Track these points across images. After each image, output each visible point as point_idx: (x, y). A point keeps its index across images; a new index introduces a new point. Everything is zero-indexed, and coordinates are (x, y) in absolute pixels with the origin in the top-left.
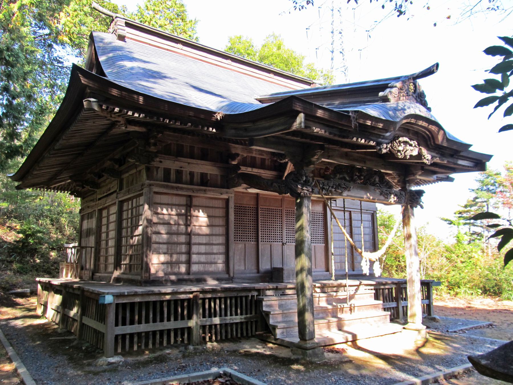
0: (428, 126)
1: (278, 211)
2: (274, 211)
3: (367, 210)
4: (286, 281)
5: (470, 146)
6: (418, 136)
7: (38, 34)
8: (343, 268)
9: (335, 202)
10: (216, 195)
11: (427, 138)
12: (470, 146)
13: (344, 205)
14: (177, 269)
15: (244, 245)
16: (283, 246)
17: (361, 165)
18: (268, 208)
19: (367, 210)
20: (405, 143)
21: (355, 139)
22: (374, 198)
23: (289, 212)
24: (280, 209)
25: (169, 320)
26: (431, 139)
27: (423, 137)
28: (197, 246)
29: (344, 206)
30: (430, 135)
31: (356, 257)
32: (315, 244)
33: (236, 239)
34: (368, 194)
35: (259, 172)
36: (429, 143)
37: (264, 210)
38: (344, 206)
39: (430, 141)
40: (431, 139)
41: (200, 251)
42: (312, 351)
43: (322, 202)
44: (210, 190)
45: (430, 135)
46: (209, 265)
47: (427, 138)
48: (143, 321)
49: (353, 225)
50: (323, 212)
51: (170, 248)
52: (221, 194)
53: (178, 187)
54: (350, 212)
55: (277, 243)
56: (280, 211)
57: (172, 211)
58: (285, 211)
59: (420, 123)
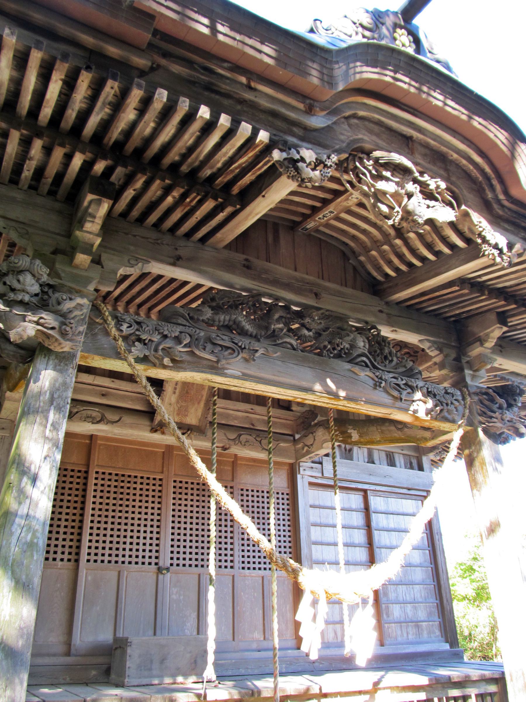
1: (152, 482)
2: (139, 480)
3: (409, 489)
4: (135, 682)
6: (446, 170)
7: (77, 313)
8: (339, 640)
9: (319, 466)
11: (481, 179)
13: (335, 471)
15: (116, 574)
16: (161, 577)
18: (121, 473)
19: (409, 489)
22: (353, 394)
23: (184, 485)
24: (158, 477)
26: (495, 182)
27: (468, 175)
29: (335, 475)
30: (488, 169)
31: (387, 608)
32: (262, 572)
33: (223, 564)
35: (96, 382)
36: (490, 195)
37: (107, 477)
38: (335, 475)
39: (492, 187)
40: (495, 182)
43: (286, 468)
45: (488, 169)
47: (481, 179)
49: (374, 524)
50: (288, 491)
54: (365, 491)
55: (251, 571)
56: (158, 483)
58: (173, 484)
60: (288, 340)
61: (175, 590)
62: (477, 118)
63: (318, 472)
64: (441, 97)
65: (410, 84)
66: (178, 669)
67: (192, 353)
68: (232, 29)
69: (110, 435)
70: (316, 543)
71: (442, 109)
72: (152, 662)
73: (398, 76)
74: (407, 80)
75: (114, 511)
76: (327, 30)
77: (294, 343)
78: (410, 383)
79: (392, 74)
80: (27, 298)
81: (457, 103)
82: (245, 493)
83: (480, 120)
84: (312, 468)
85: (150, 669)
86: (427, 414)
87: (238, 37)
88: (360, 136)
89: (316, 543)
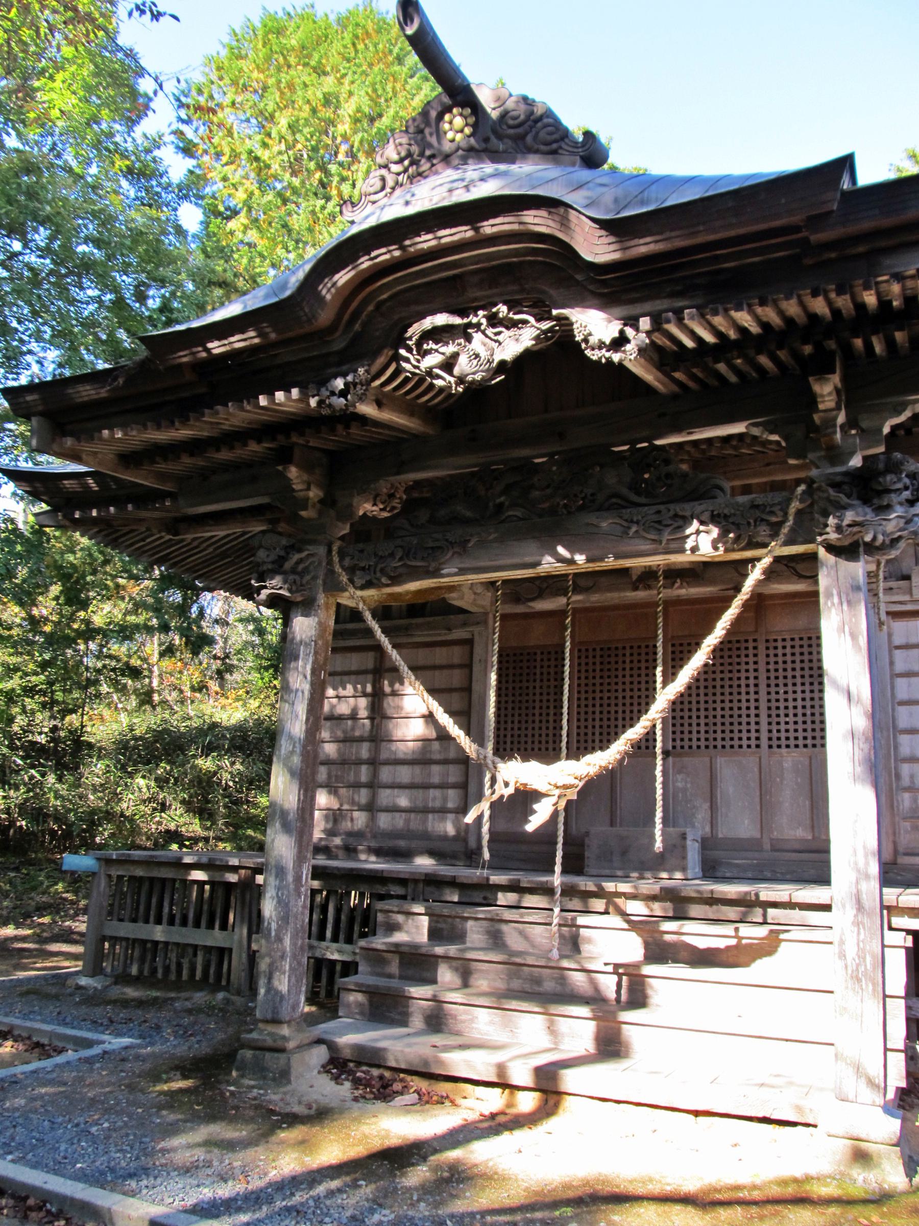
0: (477, 230)
4: (594, 872)
5: (846, 163)
10: (440, 635)
12: (846, 163)
14: (349, 824)
17: (544, 451)
20: (438, 334)
21: (263, 401)
22: (597, 553)
25: (210, 926)
28: (391, 768)
34: (561, 550)
41: (398, 780)
42: (254, 1056)
44: (418, 626)
46: (436, 815)
48: (203, 923)
51: (334, 773)
52: (449, 629)
53: (346, 630)
55: (792, 749)
57: (344, 688)
59: (425, 241)
60: (511, 513)
61: (679, 777)
62: (485, 223)
63: (904, 593)
64: (430, 236)
65: (389, 251)
66: (642, 863)
67: (404, 565)
68: (219, 339)
69: (588, 605)
70: (902, 703)
71: (439, 245)
72: (612, 853)
73: (373, 254)
74: (383, 250)
75: (722, 672)
76: (383, 188)
77: (519, 514)
78: (681, 513)
79: (367, 257)
80: (270, 567)
81: (451, 227)
82: (772, 644)
83: (491, 222)
84: (891, 589)
85: (611, 861)
86: (716, 548)
87: (226, 342)
88: (396, 317)
89: (902, 703)
